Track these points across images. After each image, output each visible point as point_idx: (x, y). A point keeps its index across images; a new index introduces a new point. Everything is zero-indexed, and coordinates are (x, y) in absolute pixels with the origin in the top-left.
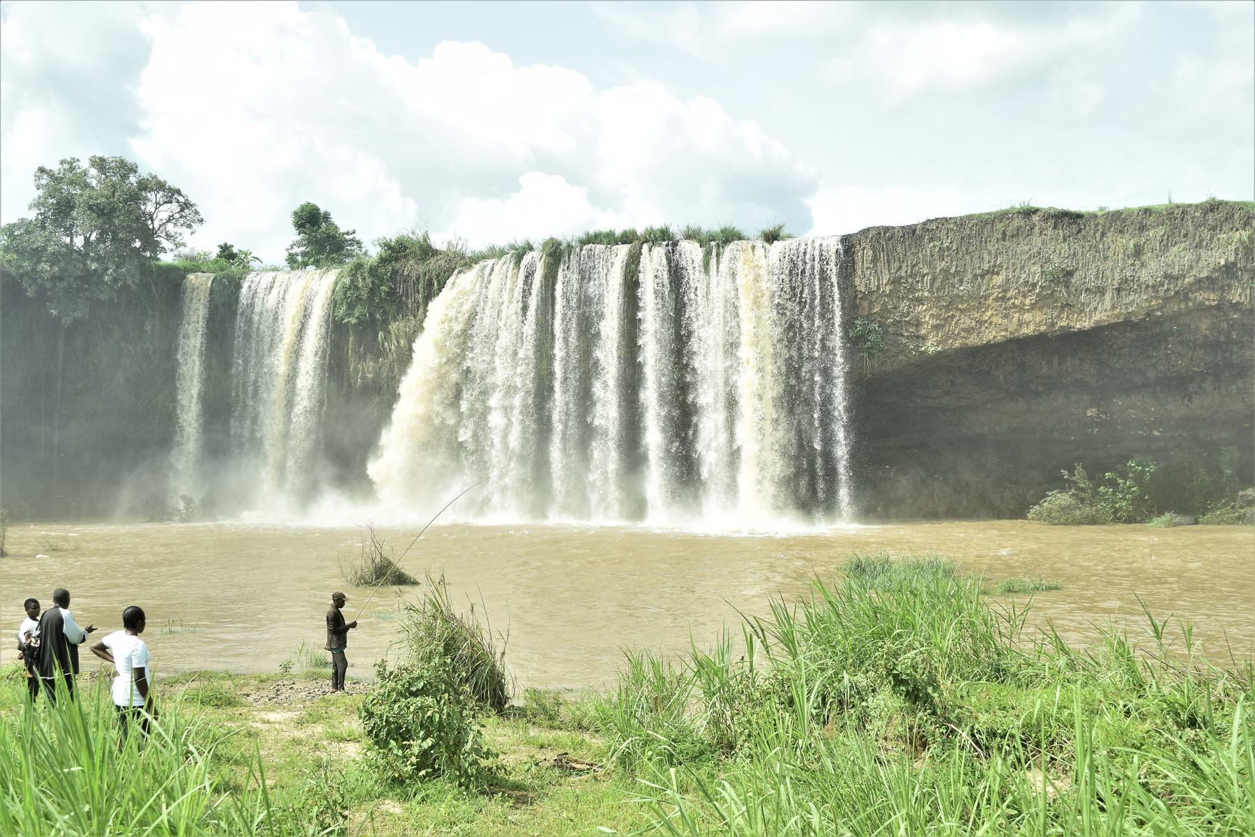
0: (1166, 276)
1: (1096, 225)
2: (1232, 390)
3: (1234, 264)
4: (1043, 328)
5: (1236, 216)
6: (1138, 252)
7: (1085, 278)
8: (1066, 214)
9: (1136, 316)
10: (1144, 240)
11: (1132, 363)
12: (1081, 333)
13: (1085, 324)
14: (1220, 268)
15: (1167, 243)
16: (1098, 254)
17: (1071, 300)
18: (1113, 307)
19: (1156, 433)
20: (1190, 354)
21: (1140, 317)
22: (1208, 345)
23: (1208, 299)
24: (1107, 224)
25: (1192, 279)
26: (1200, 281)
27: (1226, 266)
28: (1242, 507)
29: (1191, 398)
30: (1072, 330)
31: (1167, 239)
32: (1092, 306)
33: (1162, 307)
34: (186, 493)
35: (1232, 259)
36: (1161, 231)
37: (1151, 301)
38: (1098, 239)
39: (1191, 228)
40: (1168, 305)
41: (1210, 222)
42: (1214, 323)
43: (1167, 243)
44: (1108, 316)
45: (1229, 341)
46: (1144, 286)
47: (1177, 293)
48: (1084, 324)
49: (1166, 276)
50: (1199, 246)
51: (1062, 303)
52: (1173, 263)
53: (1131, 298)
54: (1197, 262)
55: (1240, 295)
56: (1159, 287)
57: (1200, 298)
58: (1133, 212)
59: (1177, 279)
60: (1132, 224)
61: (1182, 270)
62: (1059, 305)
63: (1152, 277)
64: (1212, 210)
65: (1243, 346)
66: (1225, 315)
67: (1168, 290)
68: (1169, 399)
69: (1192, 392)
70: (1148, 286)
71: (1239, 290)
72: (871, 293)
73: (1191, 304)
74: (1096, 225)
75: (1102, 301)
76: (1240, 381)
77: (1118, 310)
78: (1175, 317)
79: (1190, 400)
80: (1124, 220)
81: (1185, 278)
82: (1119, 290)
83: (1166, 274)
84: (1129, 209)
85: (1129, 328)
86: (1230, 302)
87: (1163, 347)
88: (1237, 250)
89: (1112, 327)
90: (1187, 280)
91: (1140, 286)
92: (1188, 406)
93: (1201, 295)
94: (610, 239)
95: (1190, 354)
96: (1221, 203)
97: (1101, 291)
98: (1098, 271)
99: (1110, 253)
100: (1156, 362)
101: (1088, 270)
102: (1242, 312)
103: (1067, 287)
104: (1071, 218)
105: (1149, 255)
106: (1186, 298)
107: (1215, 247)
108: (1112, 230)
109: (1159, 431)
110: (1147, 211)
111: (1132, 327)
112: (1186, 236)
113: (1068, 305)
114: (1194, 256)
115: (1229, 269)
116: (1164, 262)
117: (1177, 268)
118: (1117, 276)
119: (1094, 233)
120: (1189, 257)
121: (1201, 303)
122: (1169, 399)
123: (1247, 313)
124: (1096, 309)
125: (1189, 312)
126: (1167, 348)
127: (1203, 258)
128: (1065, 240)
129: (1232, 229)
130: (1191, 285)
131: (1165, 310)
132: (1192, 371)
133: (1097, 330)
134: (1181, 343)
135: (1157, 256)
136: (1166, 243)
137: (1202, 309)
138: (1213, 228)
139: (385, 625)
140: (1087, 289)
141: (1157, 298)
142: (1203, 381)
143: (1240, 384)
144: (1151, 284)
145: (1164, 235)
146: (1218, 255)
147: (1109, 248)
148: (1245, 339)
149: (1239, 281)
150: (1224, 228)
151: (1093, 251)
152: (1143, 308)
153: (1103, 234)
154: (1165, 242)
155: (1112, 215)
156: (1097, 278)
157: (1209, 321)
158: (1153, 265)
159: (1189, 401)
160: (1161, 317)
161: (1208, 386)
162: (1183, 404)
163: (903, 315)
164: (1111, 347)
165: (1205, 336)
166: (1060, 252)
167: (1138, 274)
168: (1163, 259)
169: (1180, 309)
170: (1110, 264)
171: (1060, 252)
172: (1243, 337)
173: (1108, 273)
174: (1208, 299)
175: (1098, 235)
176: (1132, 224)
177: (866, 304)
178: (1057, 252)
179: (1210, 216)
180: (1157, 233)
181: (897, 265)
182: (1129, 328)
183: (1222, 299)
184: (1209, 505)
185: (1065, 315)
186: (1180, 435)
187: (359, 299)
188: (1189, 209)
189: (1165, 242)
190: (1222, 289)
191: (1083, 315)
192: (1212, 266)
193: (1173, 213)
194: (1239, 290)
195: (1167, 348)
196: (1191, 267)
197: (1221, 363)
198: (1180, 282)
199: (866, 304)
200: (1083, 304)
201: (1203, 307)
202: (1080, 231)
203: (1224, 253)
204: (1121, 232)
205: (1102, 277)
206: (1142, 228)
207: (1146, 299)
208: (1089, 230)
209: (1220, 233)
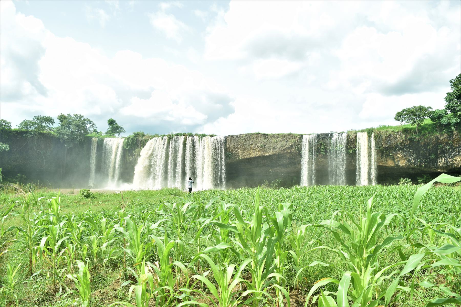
0: (281, 147)
4: (260, 155)
18: (272, 152)
49: (281, 147)
72: (230, 147)
75: (271, 150)
78: (283, 154)
94: (181, 135)
97: (270, 149)
99: (272, 142)
115: (292, 146)
121: (287, 152)
163: (236, 152)
177: (229, 149)
179: (289, 136)
180: (280, 139)
181: (234, 142)
187: (129, 144)
199: (229, 149)
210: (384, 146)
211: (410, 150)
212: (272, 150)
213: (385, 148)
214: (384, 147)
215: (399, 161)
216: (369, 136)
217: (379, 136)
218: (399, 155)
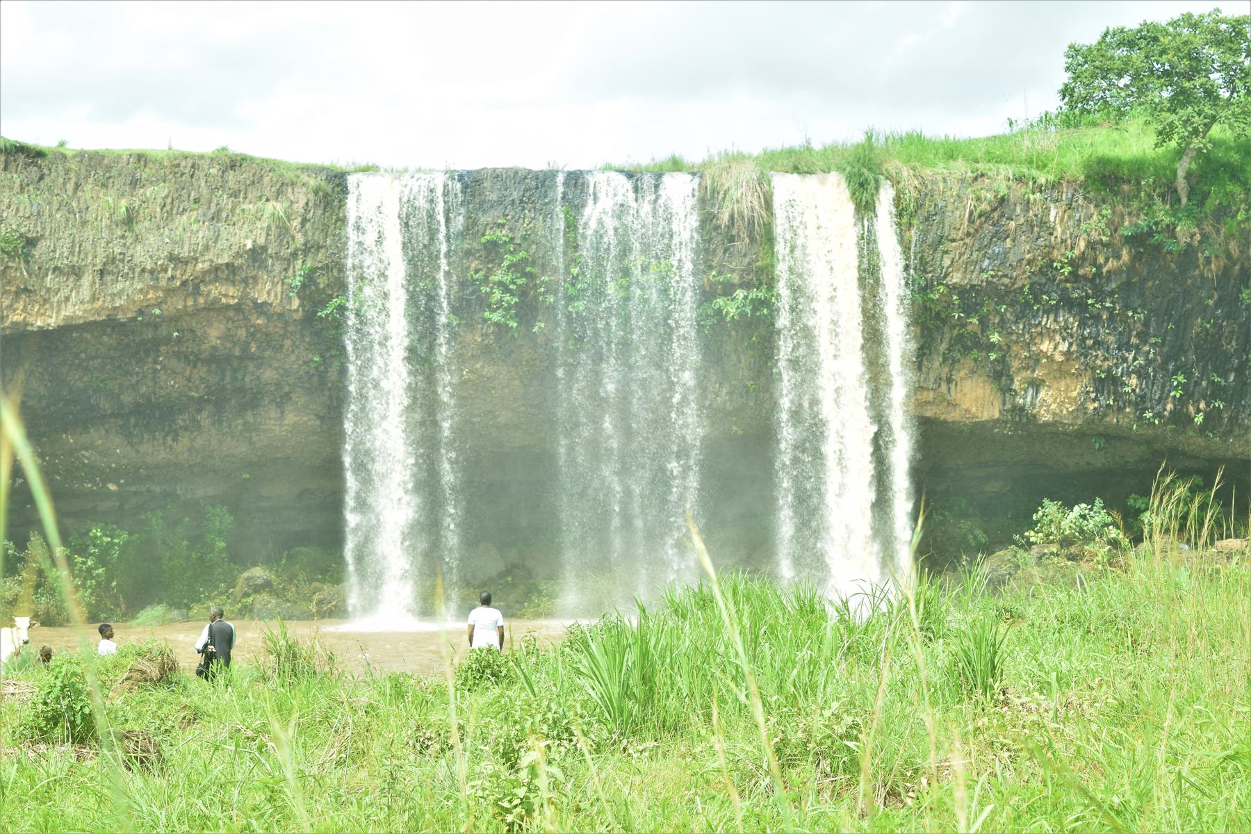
0: (172, 258)
1: (67, 172)
2: (237, 426)
3: (264, 249)
5: (266, 180)
6: (130, 220)
7: (54, 251)
8: (21, 149)
9: (124, 314)
10: (138, 203)
11: (102, 381)
12: (44, 333)
13: (52, 321)
14: (246, 252)
15: (172, 209)
16: (72, 216)
17: (32, 283)
18: (94, 298)
19: (112, 487)
20: (188, 372)
21: (130, 315)
22: (216, 360)
23: (226, 296)
24: (83, 170)
25: (206, 266)
26: (217, 268)
27: (253, 250)
28: (246, 595)
29: (177, 435)
30: (29, 328)
31: (172, 203)
32: (61, 295)
33: (161, 303)
34: (1025, 555)
35: (261, 241)
36: (162, 190)
37: (147, 293)
38: (70, 193)
39: (205, 191)
40: (169, 299)
41: (230, 184)
42: (229, 330)
43: (172, 209)
44: (85, 311)
45: (245, 356)
46: (138, 270)
47: (184, 283)
48: (49, 321)
49: (172, 258)
50: (216, 217)
51: (18, 287)
52: (182, 240)
53: (119, 286)
54: (216, 242)
55: (269, 293)
56: (159, 272)
57: (215, 293)
58: (120, 156)
59: (186, 263)
60: (120, 175)
61: (195, 251)
62: (14, 289)
63: (151, 257)
64: (233, 167)
65: (262, 364)
66: (245, 318)
67: (173, 278)
68: (146, 436)
69: (180, 428)
70: (143, 270)
71: (268, 286)
73: (201, 300)
74: (67, 172)
75: (77, 287)
76: (250, 413)
77: (100, 303)
78: (175, 319)
79: (175, 440)
80: (109, 168)
81: (197, 263)
82: (102, 273)
83: (171, 254)
84: (112, 152)
85: (109, 330)
86: (255, 302)
87: (150, 359)
88: (269, 228)
89: (88, 326)
90: (200, 266)
91: (132, 269)
92: (171, 447)
93: (216, 288)
95: (188, 372)
96: (244, 159)
97: (76, 272)
98: (73, 242)
99: (90, 217)
100: (137, 382)
101: (58, 239)
102: (269, 317)
103: (27, 262)
104: (28, 156)
105: (147, 224)
106: (196, 292)
107: (239, 221)
108: (91, 180)
109: (118, 484)
110: (141, 158)
111: (113, 328)
112: (196, 201)
113: (26, 290)
114: (212, 233)
115: (257, 254)
116: (169, 238)
117: (186, 247)
118: (100, 251)
119: (64, 184)
120: (203, 233)
121: (216, 301)
122: (146, 436)
123: (275, 318)
124: (67, 299)
125: (198, 311)
126: (155, 362)
127: (224, 235)
128: (22, 189)
129: (260, 198)
130: (205, 273)
131: (164, 306)
132: (186, 396)
133: (66, 329)
134: (178, 355)
135: (159, 227)
136: (170, 210)
137: (215, 308)
138: (235, 194)
139: (291, 732)
140: (56, 269)
141: (156, 288)
142: (199, 411)
143: (249, 417)
144: (148, 267)
145: (167, 197)
146: (243, 234)
147: (87, 208)
148: (267, 354)
149: (269, 272)
150: (250, 196)
151: (64, 211)
152: (135, 302)
153: (77, 186)
154: (168, 207)
155: (90, 159)
156: (72, 253)
157: (222, 327)
158: (151, 239)
159: (174, 440)
160: (158, 316)
161: (204, 418)
162: (164, 443)
164: (77, 356)
165: (214, 348)
166: (18, 209)
167: (130, 252)
168: (167, 232)
169: (186, 306)
170: (89, 233)
171: (18, 209)
172: (264, 350)
173: (88, 246)
174: (226, 296)
175: (70, 186)
176: (120, 175)
178: (14, 207)
179: (231, 175)
180: (157, 192)
182: (109, 330)
183: (245, 296)
184: (203, 593)
185: (20, 305)
186: (149, 491)
188: (201, 162)
189: (168, 207)
190: (245, 281)
191: (47, 306)
192: (235, 249)
193: (178, 166)
194: (268, 286)
195: (155, 362)
196: (207, 248)
197: (228, 386)
198: (190, 268)
200: (48, 290)
201: (217, 306)
202: (41, 178)
203: (251, 231)
204: (104, 186)
205: (80, 252)
206: (135, 183)
207: (141, 290)
208: (55, 177)
209: (244, 202)
210: (956, 278)
211: (1127, 307)
212: (86, 280)
213: (962, 291)
214: (953, 288)
215: (1036, 385)
216: (865, 208)
217: (928, 207)
218: (1046, 346)
